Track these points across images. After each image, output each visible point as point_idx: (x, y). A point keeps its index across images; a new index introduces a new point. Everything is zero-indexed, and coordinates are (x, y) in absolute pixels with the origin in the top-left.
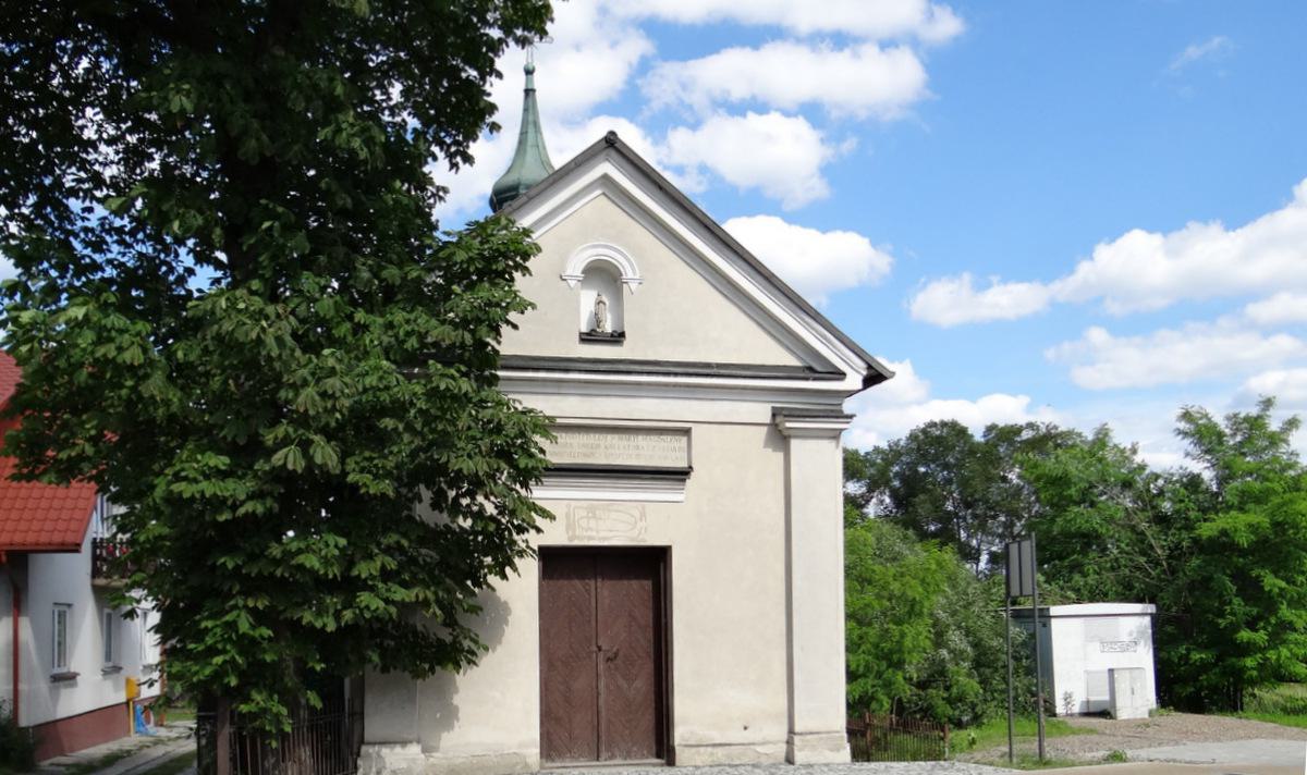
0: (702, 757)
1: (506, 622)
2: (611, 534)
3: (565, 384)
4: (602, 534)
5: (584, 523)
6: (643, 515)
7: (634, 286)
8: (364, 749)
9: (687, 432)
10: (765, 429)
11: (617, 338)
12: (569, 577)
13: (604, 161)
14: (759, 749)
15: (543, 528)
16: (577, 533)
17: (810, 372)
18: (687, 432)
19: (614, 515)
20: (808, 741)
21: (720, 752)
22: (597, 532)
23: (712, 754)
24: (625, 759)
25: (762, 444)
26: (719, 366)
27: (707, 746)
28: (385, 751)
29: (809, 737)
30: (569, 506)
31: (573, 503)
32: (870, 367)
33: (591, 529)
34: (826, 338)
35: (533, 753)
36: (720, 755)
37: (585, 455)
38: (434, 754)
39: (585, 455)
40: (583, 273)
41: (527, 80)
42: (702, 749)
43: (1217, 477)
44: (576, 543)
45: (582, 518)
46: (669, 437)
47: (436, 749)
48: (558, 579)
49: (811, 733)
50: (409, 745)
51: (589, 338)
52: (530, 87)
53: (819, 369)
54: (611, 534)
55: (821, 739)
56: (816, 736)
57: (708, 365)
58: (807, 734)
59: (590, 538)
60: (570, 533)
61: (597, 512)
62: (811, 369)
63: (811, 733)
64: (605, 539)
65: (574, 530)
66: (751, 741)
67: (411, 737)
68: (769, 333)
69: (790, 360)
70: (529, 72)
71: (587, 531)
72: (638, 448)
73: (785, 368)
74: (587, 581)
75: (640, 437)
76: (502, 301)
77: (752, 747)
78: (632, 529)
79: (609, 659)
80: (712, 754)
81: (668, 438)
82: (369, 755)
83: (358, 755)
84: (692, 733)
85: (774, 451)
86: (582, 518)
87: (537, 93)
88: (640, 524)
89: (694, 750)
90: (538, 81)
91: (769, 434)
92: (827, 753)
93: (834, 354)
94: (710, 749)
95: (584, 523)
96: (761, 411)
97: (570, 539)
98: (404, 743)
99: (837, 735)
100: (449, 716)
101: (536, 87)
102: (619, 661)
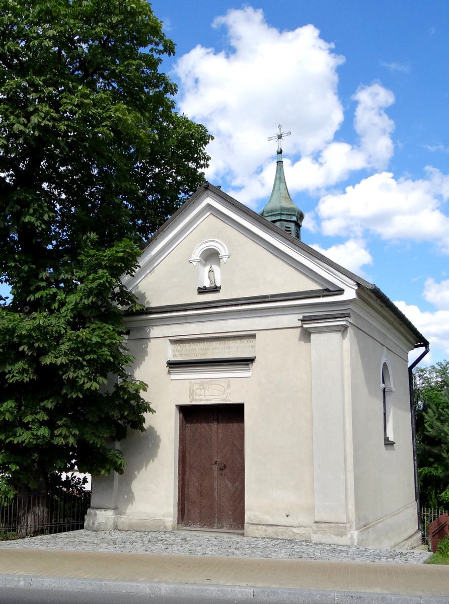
0: (260, 532)
1: (158, 447)
3: (189, 317)
6: (229, 386)
7: (225, 259)
8: (89, 510)
10: (299, 330)
11: (215, 289)
12: (201, 422)
13: (207, 197)
14: (295, 530)
17: (327, 292)
18: (253, 336)
19: (213, 386)
20: (321, 527)
21: (270, 529)
23: (265, 531)
24: (229, 529)
25: (298, 339)
26: (272, 296)
27: (263, 525)
28: (98, 512)
29: (323, 525)
30: (190, 383)
32: (358, 284)
33: (201, 395)
36: (270, 531)
38: (122, 516)
39: (203, 354)
42: (260, 527)
43: (111, 305)
44: (194, 403)
45: (197, 389)
46: (246, 340)
47: (124, 513)
48: (196, 423)
49: (325, 523)
50: (107, 510)
53: (332, 289)
55: (331, 527)
56: (327, 525)
58: (322, 523)
59: (201, 400)
62: (328, 290)
63: (325, 523)
64: (208, 400)
65: (193, 396)
66: (291, 525)
68: (302, 273)
69: (316, 287)
71: (199, 396)
73: (312, 291)
74: (210, 424)
75: (231, 342)
79: (221, 469)
80: (265, 531)
81: (245, 341)
82: (90, 514)
83: (86, 513)
85: (305, 343)
86: (197, 389)
88: (227, 391)
89: (255, 527)
91: (301, 332)
92: (333, 536)
93: (336, 280)
94: (264, 527)
95: (198, 391)
96: (293, 319)
98: (106, 509)
99: (342, 525)
100: (130, 498)
102: (226, 470)
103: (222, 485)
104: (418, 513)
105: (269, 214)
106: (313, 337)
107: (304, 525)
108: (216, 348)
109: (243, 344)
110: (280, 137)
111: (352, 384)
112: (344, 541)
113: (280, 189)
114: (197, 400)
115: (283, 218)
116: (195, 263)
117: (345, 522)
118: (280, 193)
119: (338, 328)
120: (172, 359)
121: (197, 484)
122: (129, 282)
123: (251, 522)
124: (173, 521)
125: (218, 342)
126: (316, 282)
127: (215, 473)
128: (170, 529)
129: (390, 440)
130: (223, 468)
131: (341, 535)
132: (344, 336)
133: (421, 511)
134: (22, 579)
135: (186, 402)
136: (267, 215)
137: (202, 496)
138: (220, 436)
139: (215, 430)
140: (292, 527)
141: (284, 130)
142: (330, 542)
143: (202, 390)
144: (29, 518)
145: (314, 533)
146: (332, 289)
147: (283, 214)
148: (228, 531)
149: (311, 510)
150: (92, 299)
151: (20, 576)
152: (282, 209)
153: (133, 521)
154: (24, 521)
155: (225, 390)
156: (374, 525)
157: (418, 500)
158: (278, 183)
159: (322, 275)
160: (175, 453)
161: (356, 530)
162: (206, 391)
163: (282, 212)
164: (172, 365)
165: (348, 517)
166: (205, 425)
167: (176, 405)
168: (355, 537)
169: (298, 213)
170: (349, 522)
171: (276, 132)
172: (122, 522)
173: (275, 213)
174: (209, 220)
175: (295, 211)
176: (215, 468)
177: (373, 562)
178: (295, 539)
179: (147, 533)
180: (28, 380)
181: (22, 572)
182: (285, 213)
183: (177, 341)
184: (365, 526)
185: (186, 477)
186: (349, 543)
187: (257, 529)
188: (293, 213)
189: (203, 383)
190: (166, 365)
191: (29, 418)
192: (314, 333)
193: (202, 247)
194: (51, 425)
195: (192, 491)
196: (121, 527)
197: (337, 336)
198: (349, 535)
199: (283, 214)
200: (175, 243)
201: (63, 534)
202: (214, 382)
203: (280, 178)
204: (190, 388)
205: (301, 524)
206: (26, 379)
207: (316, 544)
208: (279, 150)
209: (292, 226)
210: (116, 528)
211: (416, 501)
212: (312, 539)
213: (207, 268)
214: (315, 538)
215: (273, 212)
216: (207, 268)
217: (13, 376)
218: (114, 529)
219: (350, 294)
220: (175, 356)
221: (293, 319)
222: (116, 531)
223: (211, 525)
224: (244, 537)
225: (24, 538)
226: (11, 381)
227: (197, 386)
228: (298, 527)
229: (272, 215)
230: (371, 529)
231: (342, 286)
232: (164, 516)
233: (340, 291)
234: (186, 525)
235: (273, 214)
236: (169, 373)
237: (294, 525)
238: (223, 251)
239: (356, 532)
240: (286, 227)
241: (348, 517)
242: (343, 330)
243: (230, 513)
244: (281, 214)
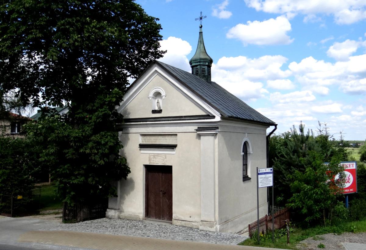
0: (179, 223)
4: (156, 162)
5: (152, 159)
6: (166, 158)
7: (164, 97)
9: (176, 135)
11: (160, 111)
13: (155, 67)
14: (193, 223)
18: (176, 135)
19: (159, 157)
20: (203, 223)
21: (183, 222)
22: (155, 161)
23: (181, 223)
24: (167, 220)
27: (180, 220)
29: (204, 222)
30: (149, 155)
31: (150, 154)
32: (221, 114)
33: (154, 161)
34: (209, 107)
36: (183, 223)
39: (155, 142)
41: (200, 30)
42: (179, 221)
44: (151, 164)
49: (205, 221)
52: (201, 31)
54: (159, 162)
55: (208, 223)
56: (206, 222)
57: (182, 117)
58: (204, 221)
59: (154, 163)
61: (156, 157)
63: (205, 221)
64: (157, 163)
67: (115, 208)
70: (201, 27)
72: (166, 139)
75: (167, 137)
76: (56, 129)
77: (191, 222)
80: (181, 223)
84: (177, 216)
87: (203, 33)
89: (177, 221)
90: (203, 29)
94: (180, 221)
96: (193, 128)
97: (150, 163)
101: (202, 31)
103: (164, 201)
104: (268, 208)
105: (194, 62)
106: (202, 137)
107: (197, 221)
108: (160, 139)
109: (172, 138)
110: (201, 19)
111: (219, 160)
112: (213, 229)
113: (200, 48)
114: (152, 163)
115: (201, 63)
116: (150, 98)
117: (214, 221)
118: (200, 50)
119: (213, 134)
120: (141, 143)
121: (154, 200)
122: (119, 109)
123: (175, 219)
124: (143, 216)
125: (161, 137)
126: (204, 111)
127: (161, 196)
128: (142, 220)
129: (249, 177)
130: (164, 193)
131: (212, 227)
132: (215, 138)
133: (270, 207)
134: (71, 249)
135: (148, 163)
136: (193, 62)
137: (155, 205)
138: (163, 179)
139: (160, 176)
140: (192, 222)
141: (203, 15)
142: (207, 230)
143: (154, 159)
144: (81, 214)
145: (200, 226)
146: (211, 115)
147: (201, 62)
148: (167, 221)
149: (199, 215)
150: (100, 120)
151: (71, 247)
152: (201, 59)
153: (126, 215)
154: (79, 215)
155: (164, 159)
156: (232, 221)
157: (269, 202)
158: (199, 44)
159: (206, 109)
160: (143, 188)
161: (219, 225)
162: (156, 159)
163: (201, 61)
164: (142, 146)
165: (215, 219)
166: (157, 173)
167: (144, 165)
168: (218, 228)
169: (209, 60)
170: (216, 221)
171: (199, 16)
172: (122, 215)
173: (197, 61)
174: (156, 78)
175: (207, 60)
176: (161, 193)
177: (216, 243)
178: (193, 227)
179: (131, 221)
180: (75, 158)
181: (72, 245)
182: (202, 61)
183: (143, 135)
184: (225, 222)
185: (149, 196)
186: (214, 231)
187: (178, 222)
188: (206, 61)
189: (155, 156)
190: (139, 146)
191: (77, 173)
192: (202, 136)
193: (153, 91)
194: (86, 176)
195: (151, 203)
196: (121, 217)
197: (211, 138)
198: (215, 228)
199: (201, 62)
200: (136, 94)
201: (96, 221)
202: (160, 155)
203: (201, 41)
204: (149, 157)
205: (196, 221)
206: (74, 157)
207: (201, 230)
208: (200, 26)
209: (206, 67)
210: (119, 218)
211: (268, 202)
212: (199, 228)
213: (156, 101)
214: (201, 228)
215: (196, 61)
216: (156, 101)
217: (69, 156)
218: (118, 219)
219: (218, 118)
220: (143, 142)
221: (193, 128)
222: (119, 219)
223: (160, 219)
224: (172, 225)
225: (79, 222)
226: (68, 158)
227: (152, 157)
228: (195, 222)
229: (196, 62)
230: (229, 222)
231: (214, 115)
232: (139, 213)
233: (214, 117)
234: (149, 217)
235: (196, 61)
236: (140, 150)
237: (193, 221)
238: (163, 93)
239: (219, 226)
240: (203, 68)
241: (215, 219)
242: (215, 135)
243: (168, 213)
244: (200, 62)
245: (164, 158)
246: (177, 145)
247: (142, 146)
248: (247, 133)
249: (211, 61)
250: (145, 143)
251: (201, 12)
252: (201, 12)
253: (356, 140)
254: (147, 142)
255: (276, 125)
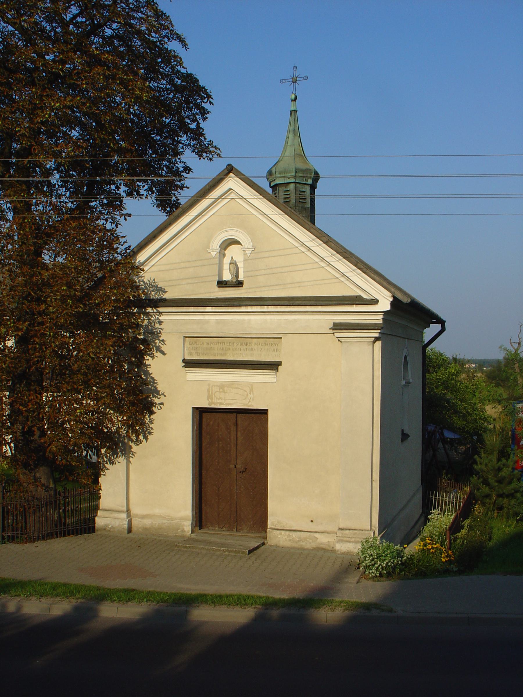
1: (437, 315)
2: (234, 401)
15: (277, 359)
16: (213, 401)
21: (294, 535)
22: (225, 400)
23: (289, 535)
29: (347, 532)
33: (221, 398)
35: (187, 526)
37: (222, 355)
39: (222, 355)
40: (220, 247)
42: (283, 532)
51: (221, 284)
54: (234, 401)
55: (355, 533)
56: (351, 531)
58: (346, 529)
59: (221, 404)
60: (210, 400)
61: (225, 389)
64: (229, 404)
65: (212, 399)
78: (245, 399)
89: (278, 532)
94: (288, 533)
95: (217, 394)
114: (217, 403)
141: (301, 72)
146: (365, 296)
155: (247, 395)
162: (227, 394)
171: (289, 74)
187: (281, 534)
204: (208, 391)
208: (293, 97)
231: (377, 297)
232: (182, 519)
233: (375, 302)
245: (248, 391)
246: (281, 362)
247: (189, 364)
248: (408, 339)
249: (316, 178)
250: (195, 357)
251: (295, 67)
252: (295, 67)
253: (486, 358)
254: (203, 354)
255: (442, 322)
